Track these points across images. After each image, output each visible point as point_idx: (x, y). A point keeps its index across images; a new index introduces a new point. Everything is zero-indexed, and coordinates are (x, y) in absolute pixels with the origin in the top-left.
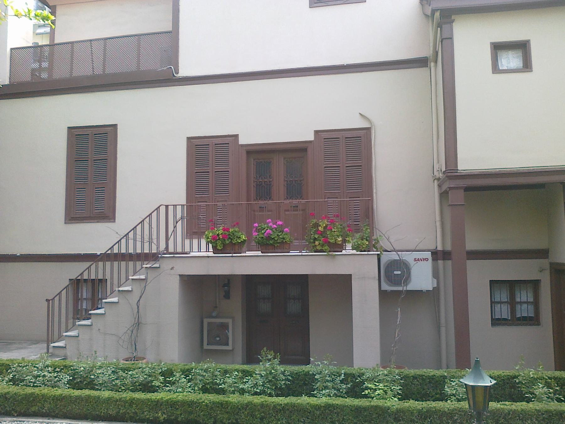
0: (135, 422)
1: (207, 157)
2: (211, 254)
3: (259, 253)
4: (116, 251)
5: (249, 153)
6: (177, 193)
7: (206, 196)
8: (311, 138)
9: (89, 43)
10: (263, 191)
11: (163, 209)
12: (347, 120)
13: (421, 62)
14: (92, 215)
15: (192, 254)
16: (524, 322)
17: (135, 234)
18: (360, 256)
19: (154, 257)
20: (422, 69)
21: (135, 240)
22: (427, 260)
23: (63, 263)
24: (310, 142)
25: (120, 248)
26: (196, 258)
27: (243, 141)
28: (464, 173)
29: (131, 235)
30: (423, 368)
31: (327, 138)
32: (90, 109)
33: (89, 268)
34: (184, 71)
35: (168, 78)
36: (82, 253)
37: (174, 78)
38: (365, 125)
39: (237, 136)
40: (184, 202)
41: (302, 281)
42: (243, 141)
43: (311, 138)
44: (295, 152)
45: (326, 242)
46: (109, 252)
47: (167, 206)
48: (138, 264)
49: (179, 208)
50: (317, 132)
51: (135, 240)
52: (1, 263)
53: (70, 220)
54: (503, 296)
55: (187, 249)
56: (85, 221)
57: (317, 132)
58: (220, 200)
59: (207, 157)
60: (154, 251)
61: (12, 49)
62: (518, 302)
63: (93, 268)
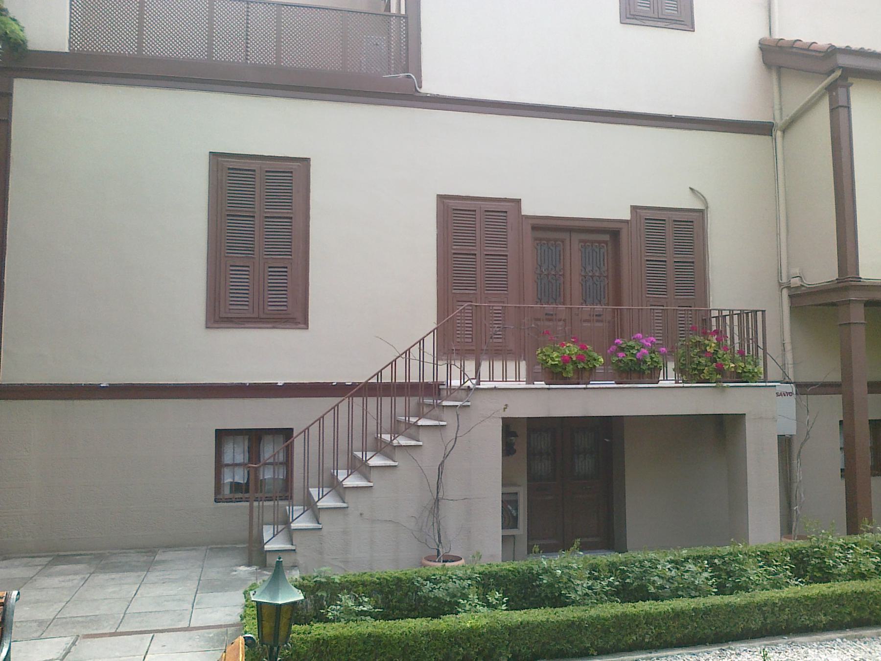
0: (551, 657)
1: (472, 232)
3: (612, 384)
4: (386, 378)
5: (535, 228)
7: (458, 291)
8: (626, 216)
10: (551, 288)
12: (673, 196)
13: (763, 129)
14: (262, 316)
16: (240, 495)
17: (422, 350)
18: (629, 390)
20: (763, 137)
21: (422, 361)
22: (790, 394)
23: (115, 401)
24: (627, 222)
25: (394, 373)
26: (513, 391)
27: (527, 209)
28: (867, 283)
29: (415, 352)
30: (651, 549)
31: (652, 221)
32: (264, 127)
34: (429, 86)
35: (406, 93)
36: (247, 381)
37: (417, 94)
38: (698, 206)
39: (519, 201)
41: (607, 429)
42: (527, 209)
44: (603, 236)
45: (720, 370)
46: (374, 380)
50: (634, 209)
51: (422, 361)
52: (3, 401)
53: (216, 322)
54: (236, 453)
56: (247, 325)
57: (634, 209)
58: (493, 300)
59: (472, 232)
62: (227, 465)
63: (344, 407)
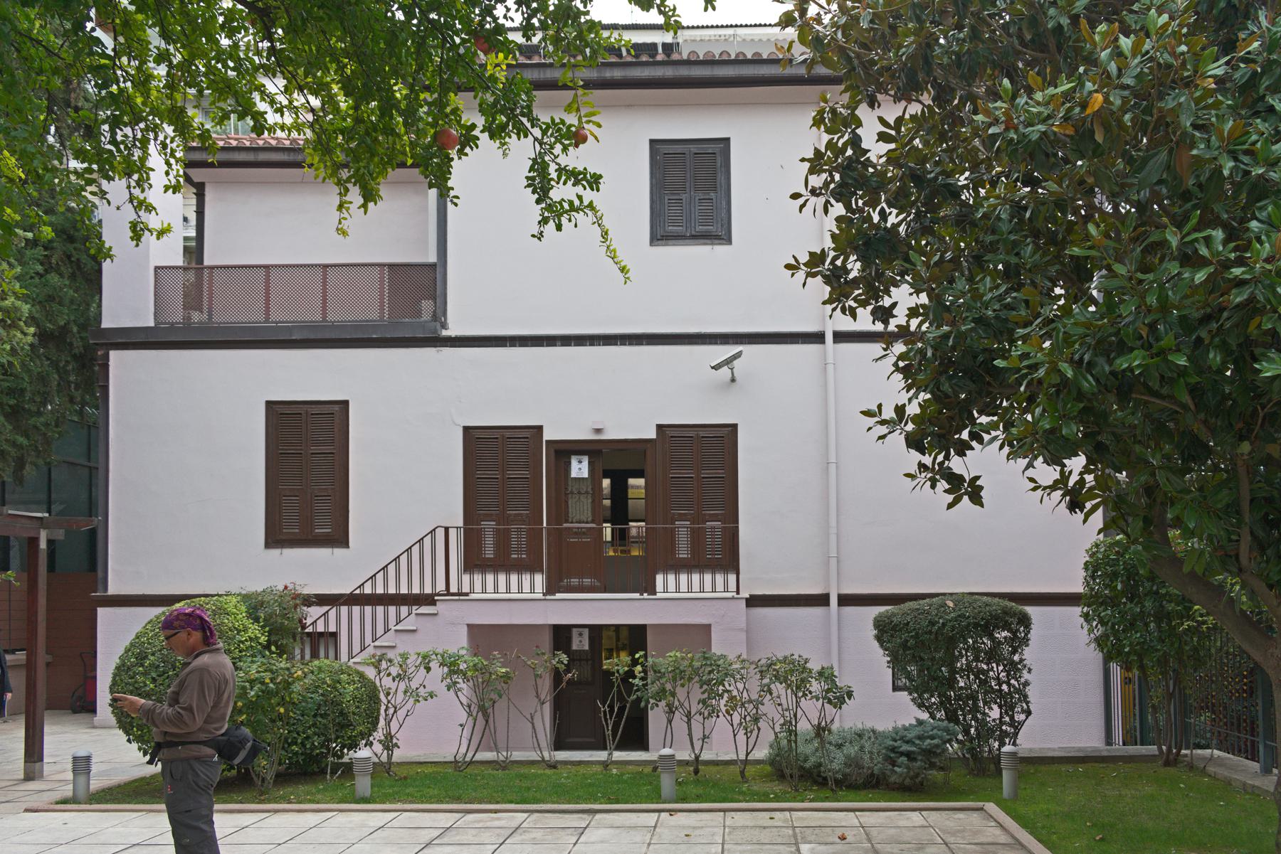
2: (1118, 748)
6: (449, 506)
9: (263, 271)
11: (440, 534)
15: (473, 596)
19: (429, 600)
27: (548, 435)
32: (307, 376)
33: (747, 754)
39: (540, 428)
40: (461, 524)
43: (652, 434)
46: (358, 592)
47: (447, 529)
48: (404, 610)
49: (452, 533)
50: (660, 427)
55: (466, 589)
57: (660, 427)
60: (428, 590)
61: (157, 268)
63: (333, 613)
